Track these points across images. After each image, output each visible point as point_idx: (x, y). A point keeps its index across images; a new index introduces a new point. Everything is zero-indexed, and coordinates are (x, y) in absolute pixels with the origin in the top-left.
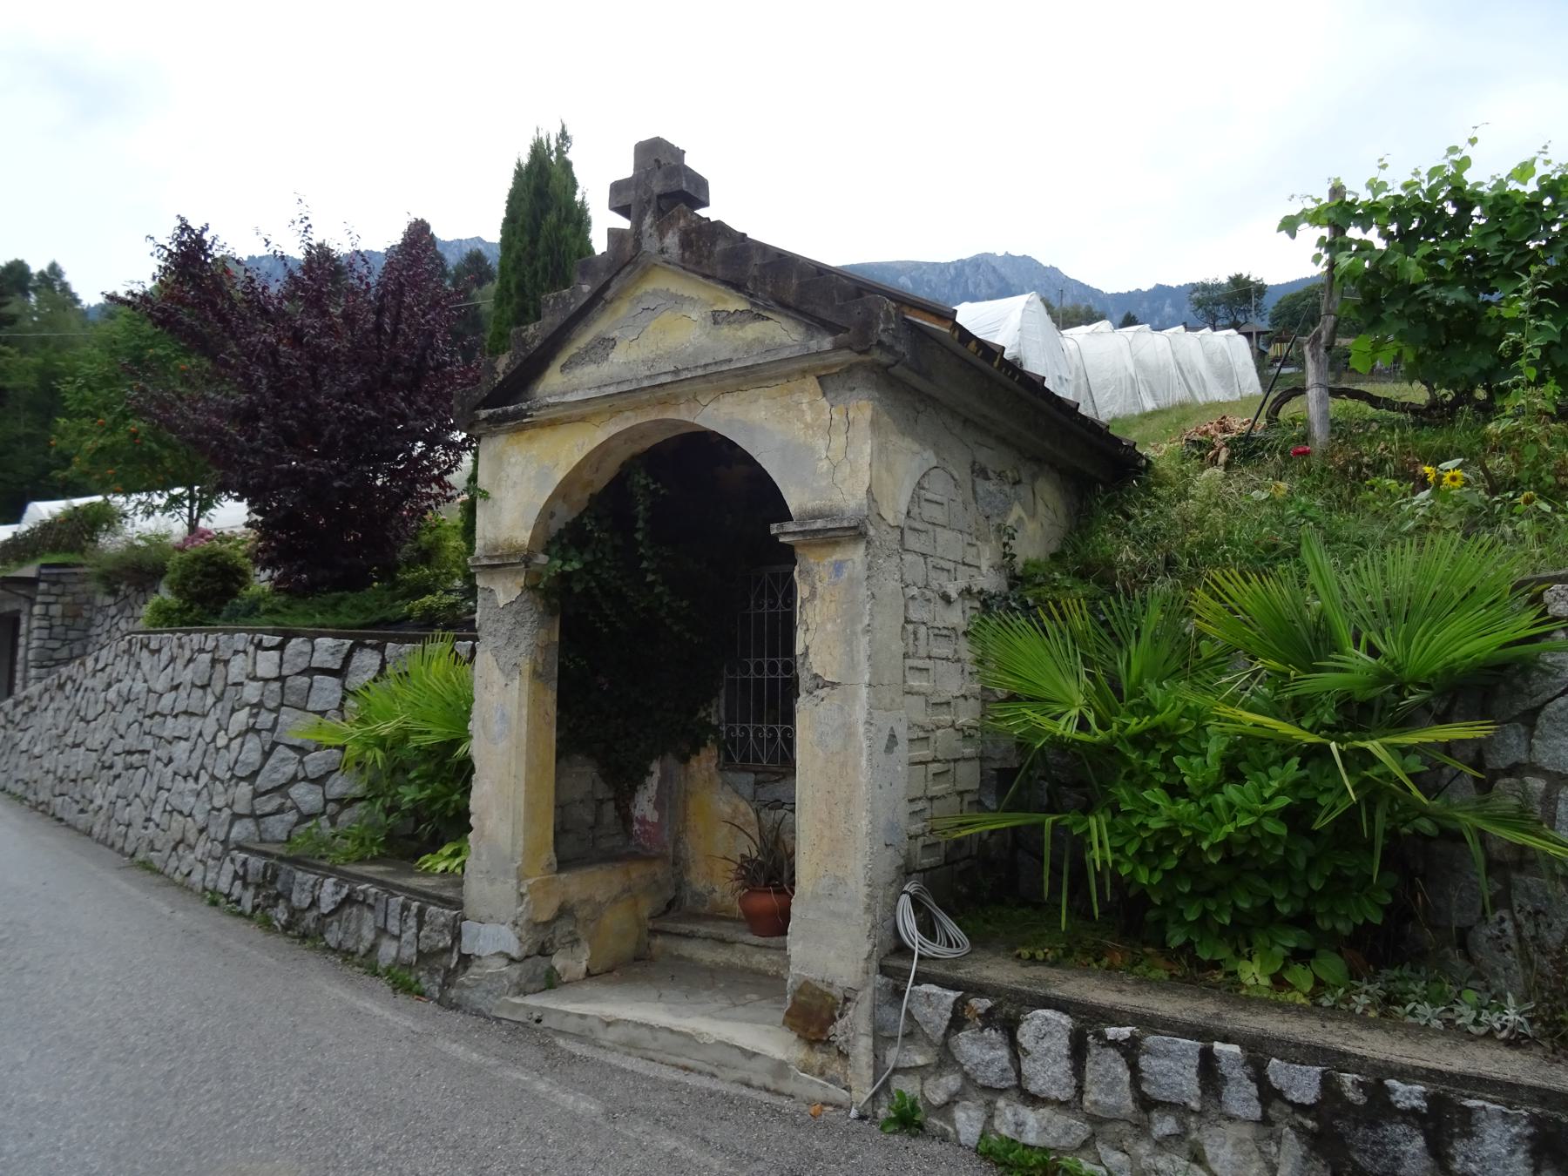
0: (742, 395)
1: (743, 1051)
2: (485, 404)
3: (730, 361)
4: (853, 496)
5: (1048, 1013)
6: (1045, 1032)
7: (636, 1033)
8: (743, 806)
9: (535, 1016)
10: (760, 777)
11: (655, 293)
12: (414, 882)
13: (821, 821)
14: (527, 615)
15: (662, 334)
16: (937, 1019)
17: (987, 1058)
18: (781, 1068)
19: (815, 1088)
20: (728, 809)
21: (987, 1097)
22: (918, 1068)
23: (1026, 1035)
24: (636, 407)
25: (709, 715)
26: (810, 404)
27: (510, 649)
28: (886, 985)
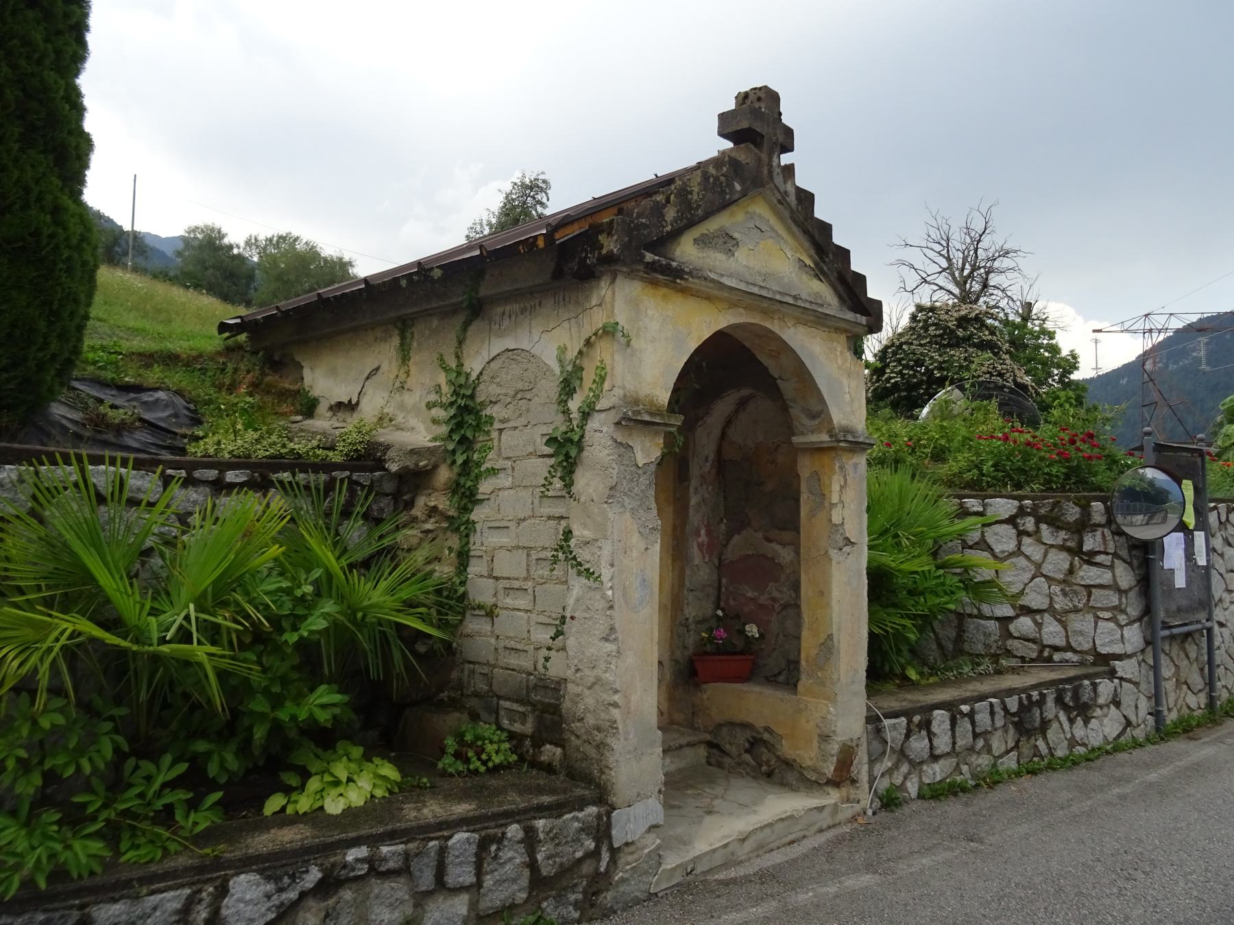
6: (940, 719)
7: (760, 836)
12: (262, 842)
26: (841, 353)
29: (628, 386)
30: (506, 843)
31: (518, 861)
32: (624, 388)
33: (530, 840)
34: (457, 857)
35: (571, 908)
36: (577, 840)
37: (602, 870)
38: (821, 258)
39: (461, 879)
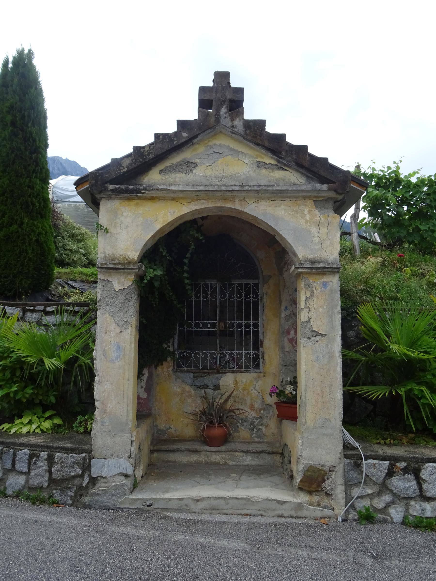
0: (272, 202)
1: (278, 502)
2: (112, 182)
3: (273, 186)
4: (332, 254)
5: (431, 464)
8: (187, 388)
9: (148, 503)
10: (196, 375)
11: (220, 145)
13: (317, 394)
14: (133, 296)
15: (226, 166)
16: (379, 474)
17: (407, 486)
18: (300, 506)
19: (317, 512)
20: (179, 390)
21: (405, 502)
22: (368, 495)
23: (424, 474)
24: (208, 199)
25: (169, 347)
26: (309, 212)
27: (121, 313)
28: (350, 463)
29: (107, 252)
30: (40, 458)
31: (44, 468)
32: (105, 253)
33: (50, 460)
34: (20, 459)
35: (69, 498)
36: (73, 467)
37: (84, 485)
38: (278, 156)
39: (21, 469)
